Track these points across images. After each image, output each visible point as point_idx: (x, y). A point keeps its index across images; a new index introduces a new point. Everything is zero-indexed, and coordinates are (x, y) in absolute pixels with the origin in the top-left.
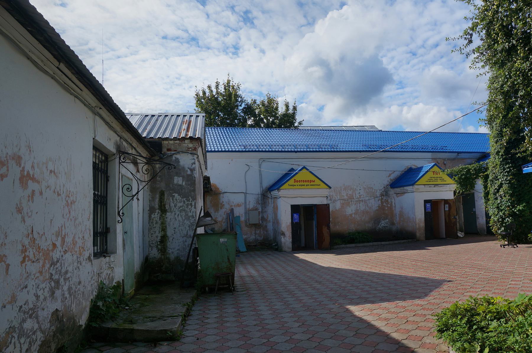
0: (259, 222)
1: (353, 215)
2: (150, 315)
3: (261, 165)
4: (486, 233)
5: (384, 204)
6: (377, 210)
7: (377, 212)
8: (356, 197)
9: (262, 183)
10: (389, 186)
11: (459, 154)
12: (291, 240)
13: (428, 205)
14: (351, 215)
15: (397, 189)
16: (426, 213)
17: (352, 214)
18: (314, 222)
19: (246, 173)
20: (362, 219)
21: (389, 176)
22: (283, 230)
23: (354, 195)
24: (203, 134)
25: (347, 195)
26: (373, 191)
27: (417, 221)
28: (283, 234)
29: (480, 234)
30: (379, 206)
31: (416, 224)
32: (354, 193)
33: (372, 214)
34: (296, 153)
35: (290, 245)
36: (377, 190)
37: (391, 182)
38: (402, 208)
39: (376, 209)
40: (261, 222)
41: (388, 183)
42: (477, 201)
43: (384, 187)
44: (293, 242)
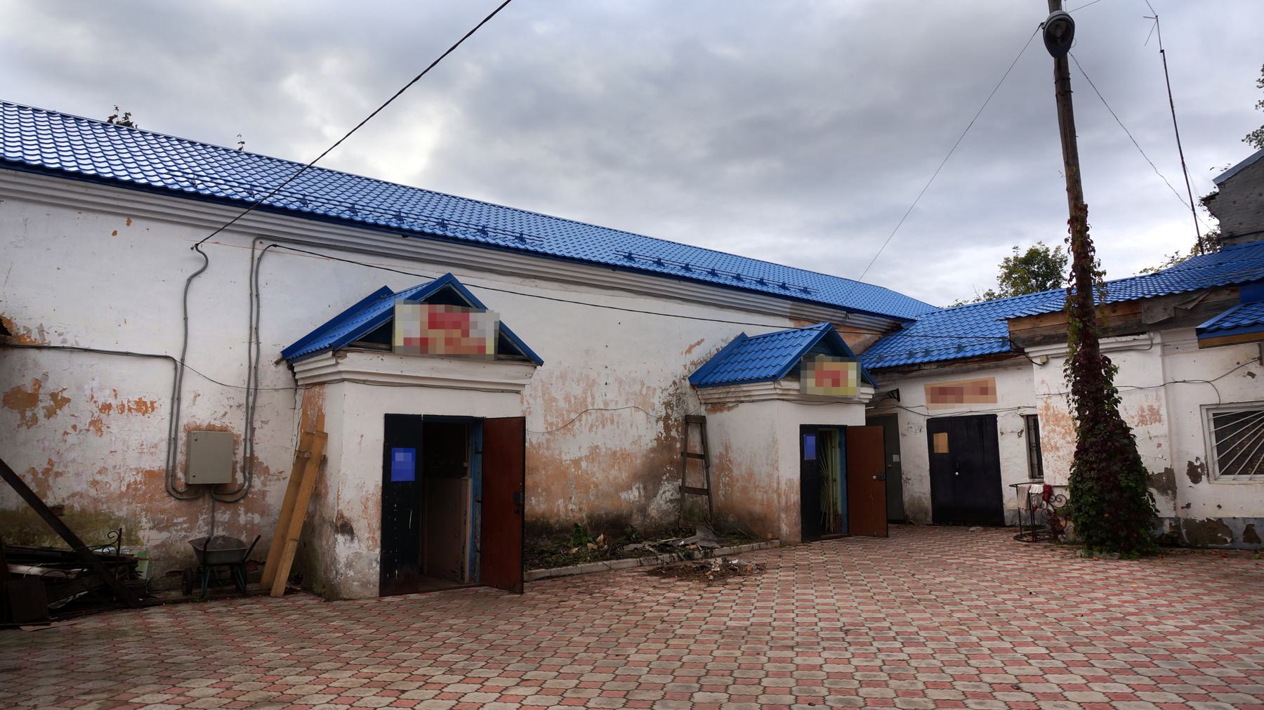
0: (234, 480)
1: (584, 464)
2: (643, 698)
3: (259, 259)
4: (930, 519)
5: (672, 434)
6: (653, 450)
7: (652, 455)
8: (593, 404)
9: (257, 328)
10: (688, 383)
11: (850, 316)
12: (378, 550)
13: (811, 440)
14: (577, 462)
15: (714, 391)
16: (804, 464)
17: (580, 459)
18: (470, 482)
19: (189, 281)
20: (611, 477)
21: (689, 351)
22: (346, 514)
23: (589, 400)
24: (1210, 335)
25: (567, 399)
26: (644, 392)
27: (783, 487)
28: (346, 528)
29: (911, 523)
30: (658, 439)
31: (779, 496)
32: (589, 394)
33: (639, 461)
34: (404, 236)
35: (374, 572)
36: (655, 389)
37: (694, 370)
38: (727, 448)
39: (650, 445)
40: (240, 477)
41: (686, 372)
42: (904, 435)
43: (675, 383)
44: (388, 562)
